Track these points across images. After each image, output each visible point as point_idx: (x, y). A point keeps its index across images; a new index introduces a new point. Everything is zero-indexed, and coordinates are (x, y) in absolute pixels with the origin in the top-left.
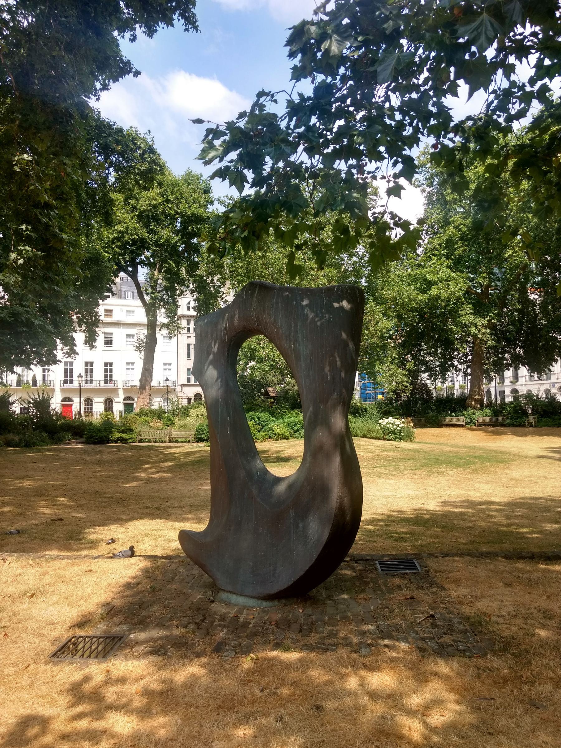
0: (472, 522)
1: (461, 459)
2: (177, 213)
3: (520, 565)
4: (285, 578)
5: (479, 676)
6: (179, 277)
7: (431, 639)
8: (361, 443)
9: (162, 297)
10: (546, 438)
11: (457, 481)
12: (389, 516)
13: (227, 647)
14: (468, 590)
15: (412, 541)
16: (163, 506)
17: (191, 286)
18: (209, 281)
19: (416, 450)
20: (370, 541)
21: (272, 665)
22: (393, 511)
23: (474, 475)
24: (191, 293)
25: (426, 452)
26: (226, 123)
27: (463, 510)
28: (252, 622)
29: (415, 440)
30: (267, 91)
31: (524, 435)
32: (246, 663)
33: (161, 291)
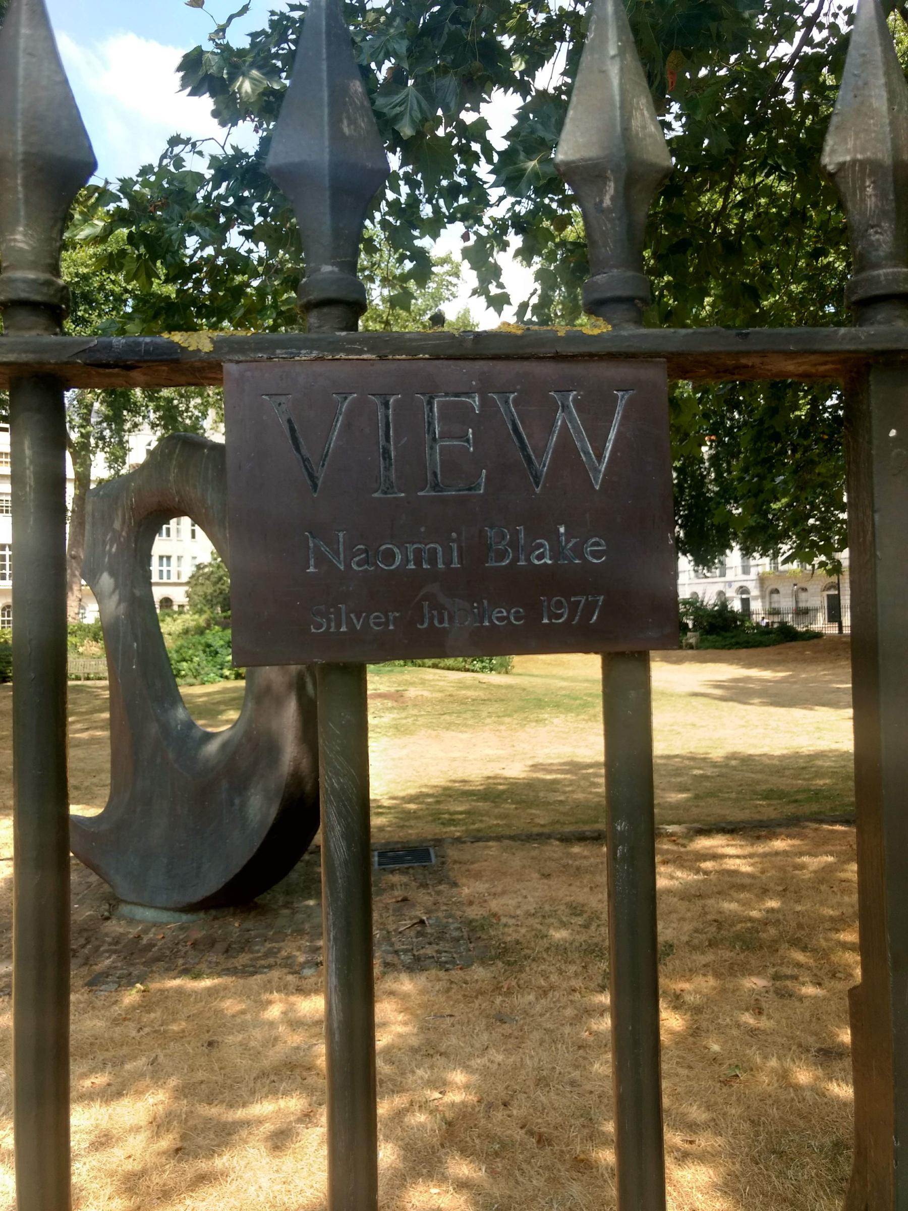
0: (565, 793)
1: (576, 699)
2: (126, 291)
3: (576, 849)
4: (213, 880)
5: (448, 990)
6: (129, 400)
7: (405, 951)
8: (427, 677)
9: (102, 432)
10: (710, 666)
11: (564, 732)
12: (446, 789)
13: (110, 979)
14: (487, 886)
15: (466, 824)
16: (86, 784)
17: (152, 416)
18: (182, 407)
19: (509, 687)
20: (402, 827)
21: (167, 997)
22: (455, 781)
23: (590, 724)
24: (152, 428)
25: (524, 690)
26: (120, 180)
27: (559, 776)
28: (159, 944)
29: (515, 671)
30: (184, 136)
31: (679, 661)
32: (131, 997)
33: (100, 423)
